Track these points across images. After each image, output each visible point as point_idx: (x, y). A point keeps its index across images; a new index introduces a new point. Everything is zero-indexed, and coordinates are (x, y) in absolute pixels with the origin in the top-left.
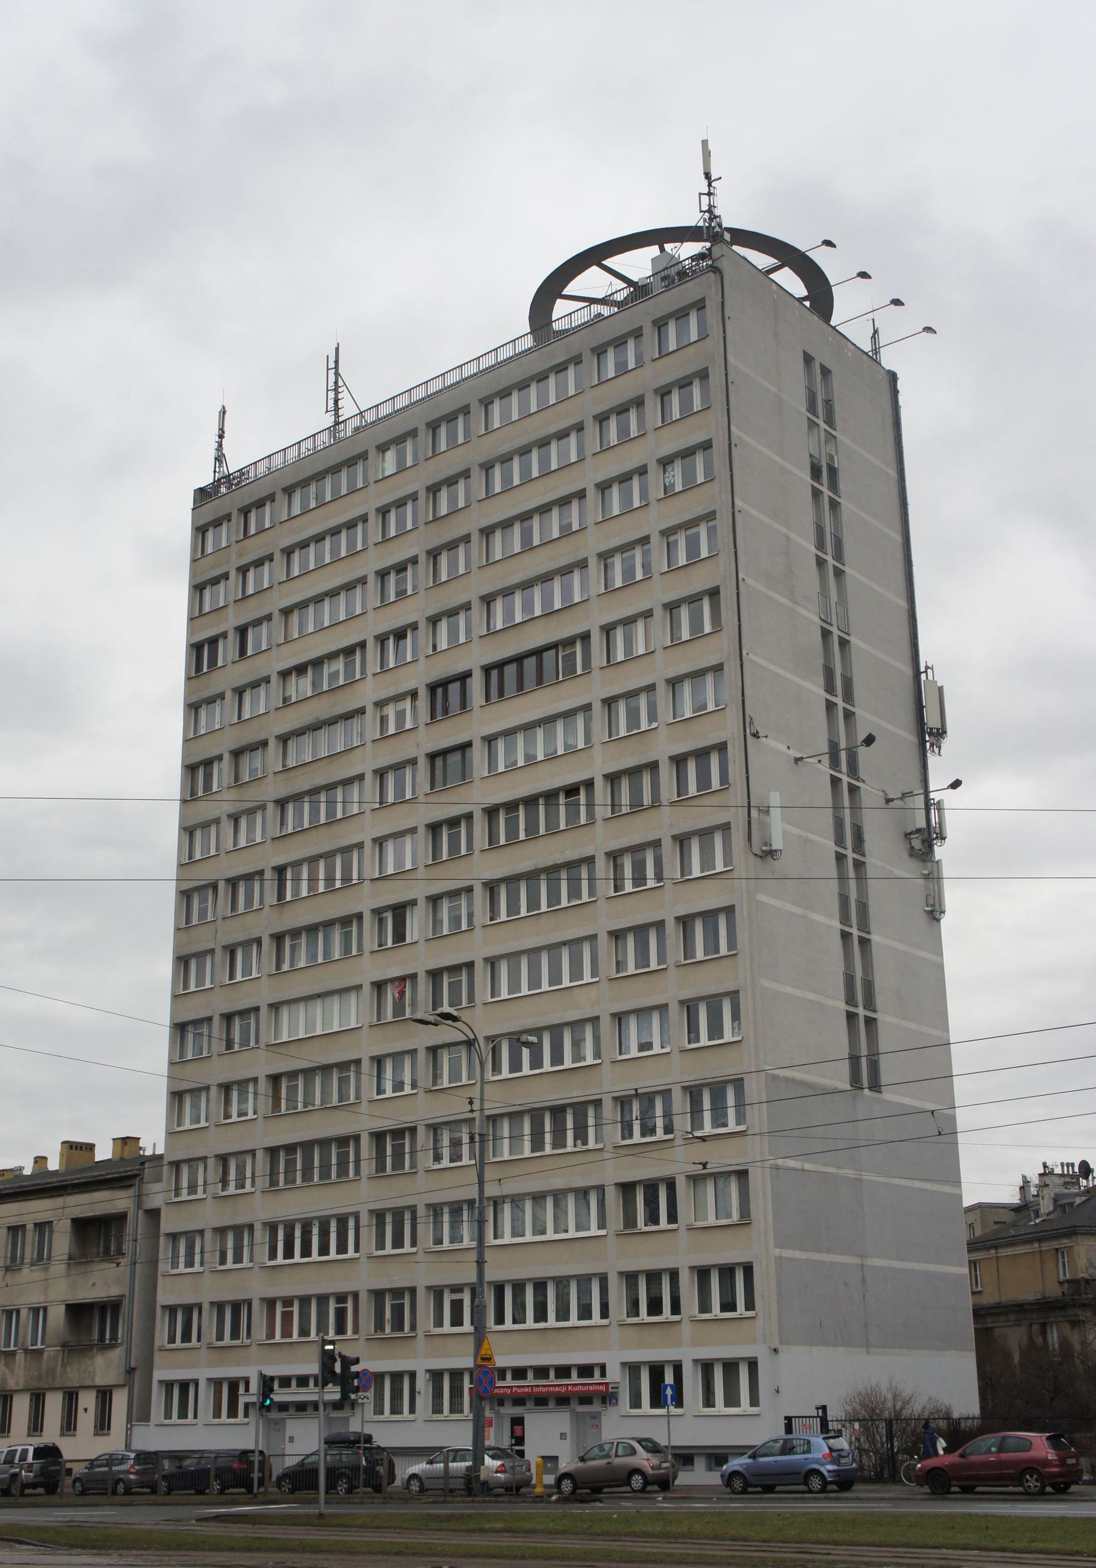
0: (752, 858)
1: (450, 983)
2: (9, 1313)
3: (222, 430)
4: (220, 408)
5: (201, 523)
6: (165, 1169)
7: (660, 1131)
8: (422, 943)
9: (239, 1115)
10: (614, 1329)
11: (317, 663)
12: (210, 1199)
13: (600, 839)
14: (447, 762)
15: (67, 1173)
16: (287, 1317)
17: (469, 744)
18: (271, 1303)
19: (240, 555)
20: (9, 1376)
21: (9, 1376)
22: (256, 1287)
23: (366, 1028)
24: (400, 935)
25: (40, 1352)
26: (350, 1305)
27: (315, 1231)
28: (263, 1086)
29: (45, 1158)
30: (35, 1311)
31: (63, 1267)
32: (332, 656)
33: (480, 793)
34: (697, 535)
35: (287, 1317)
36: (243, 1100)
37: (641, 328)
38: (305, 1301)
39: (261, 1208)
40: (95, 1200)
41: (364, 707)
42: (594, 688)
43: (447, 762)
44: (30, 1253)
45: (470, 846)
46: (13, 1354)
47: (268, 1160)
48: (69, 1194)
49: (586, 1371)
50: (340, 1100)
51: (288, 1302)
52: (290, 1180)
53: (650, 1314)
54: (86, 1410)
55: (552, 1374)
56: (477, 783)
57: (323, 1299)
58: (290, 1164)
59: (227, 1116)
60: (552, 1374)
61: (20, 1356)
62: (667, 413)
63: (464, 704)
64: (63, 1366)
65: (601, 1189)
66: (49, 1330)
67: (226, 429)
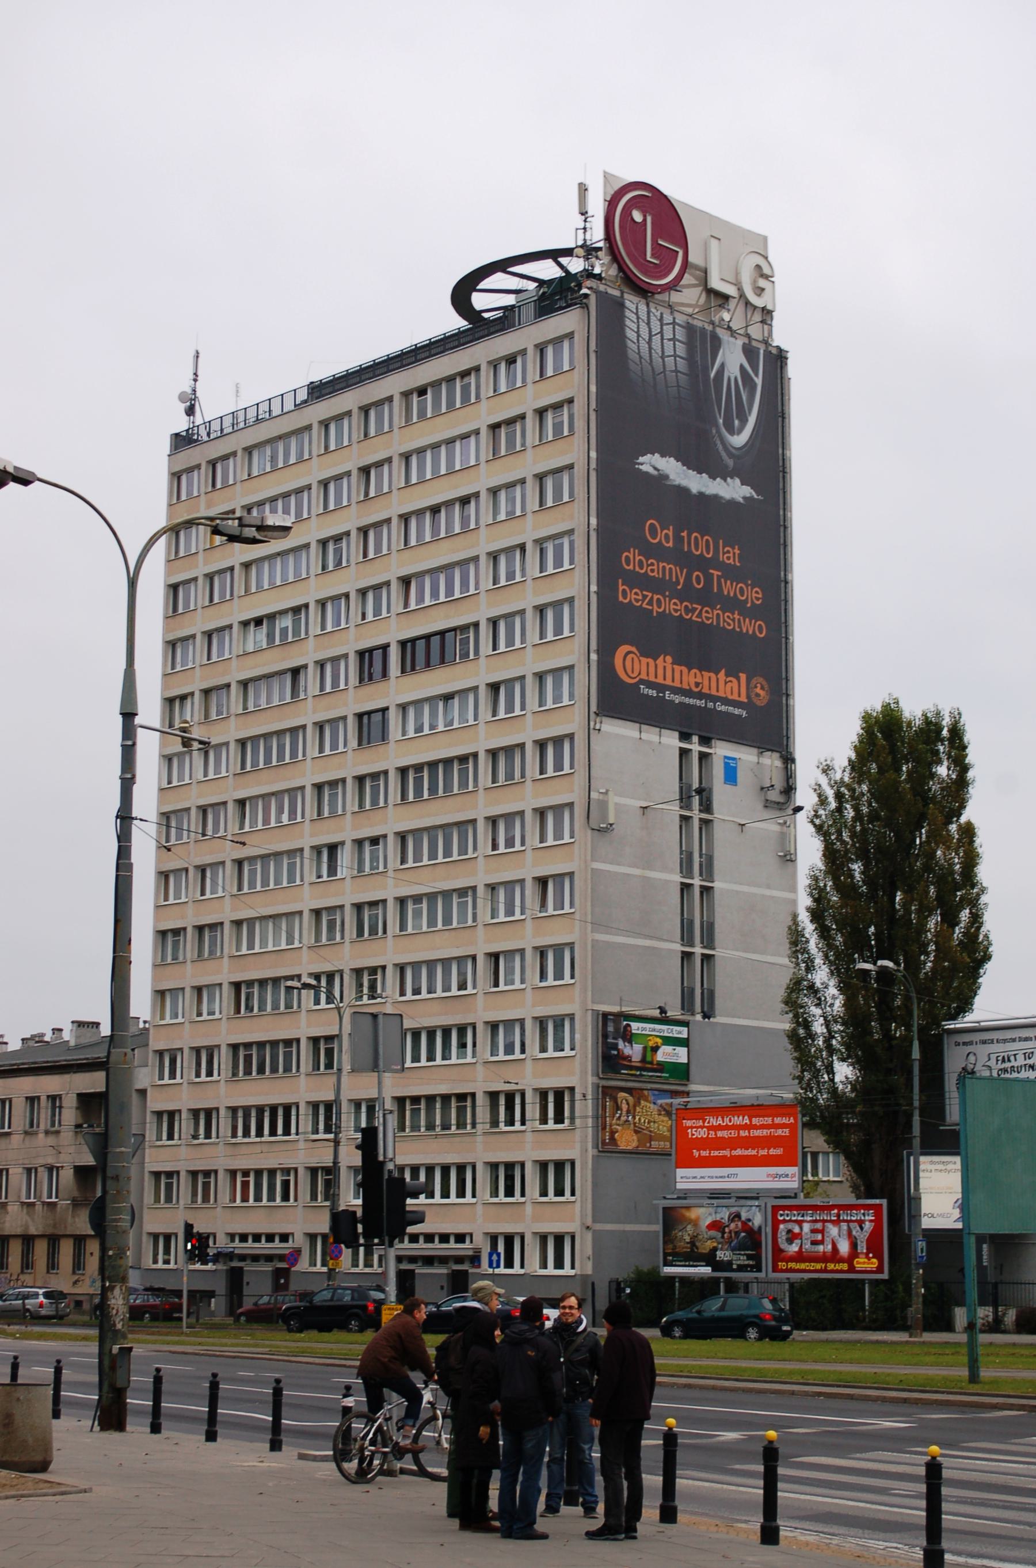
0: (589, 832)
1: (370, 915)
2: (29, 1170)
3: (196, 374)
4: (193, 353)
5: (177, 469)
6: (151, 1054)
7: (469, 1127)
8: (348, 879)
9: (209, 1014)
10: (479, 1208)
11: (272, 617)
12: (185, 1085)
13: (482, 806)
14: (371, 726)
15: (78, 1047)
16: (245, 1185)
17: (387, 708)
18: (233, 1173)
19: (209, 506)
20: (30, 1223)
21: (30, 1223)
22: (389, 889)
23: (348, 879)
24: (332, 870)
25: (54, 1204)
26: (292, 1178)
27: (267, 1114)
28: (227, 991)
29: (61, 1030)
30: (50, 1169)
31: (71, 1134)
32: (283, 612)
33: (392, 756)
34: (562, 544)
35: (245, 1185)
36: (211, 1000)
37: (526, 349)
38: (259, 1173)
39: (394, 819)
40: (93, 1080)
41: (479, 366)
42: (478, 673)
43: (371, 726)
44: (44, 1124)
45: (386, 801)
46: (33, 1204)
47: (231, 1054)
48: (75, 1072)
49: (460, 1238)
50: (286, 1008)
51: (246, 1173)
52: (248, 1072)
53: (506, 1196)
54: (92, 1254)
55: (437, 1239)
56: (392, 745)
57: (272, 1172)
58: (419, 782)
59: (199, 1014)
60: (437, 1239)
61: (39, 1207)
62: (544, 433)
63: (385, 674)
64: (73, 1217)
65: (522, 1022)
66: (60, 1187)
67: (199, 373)
